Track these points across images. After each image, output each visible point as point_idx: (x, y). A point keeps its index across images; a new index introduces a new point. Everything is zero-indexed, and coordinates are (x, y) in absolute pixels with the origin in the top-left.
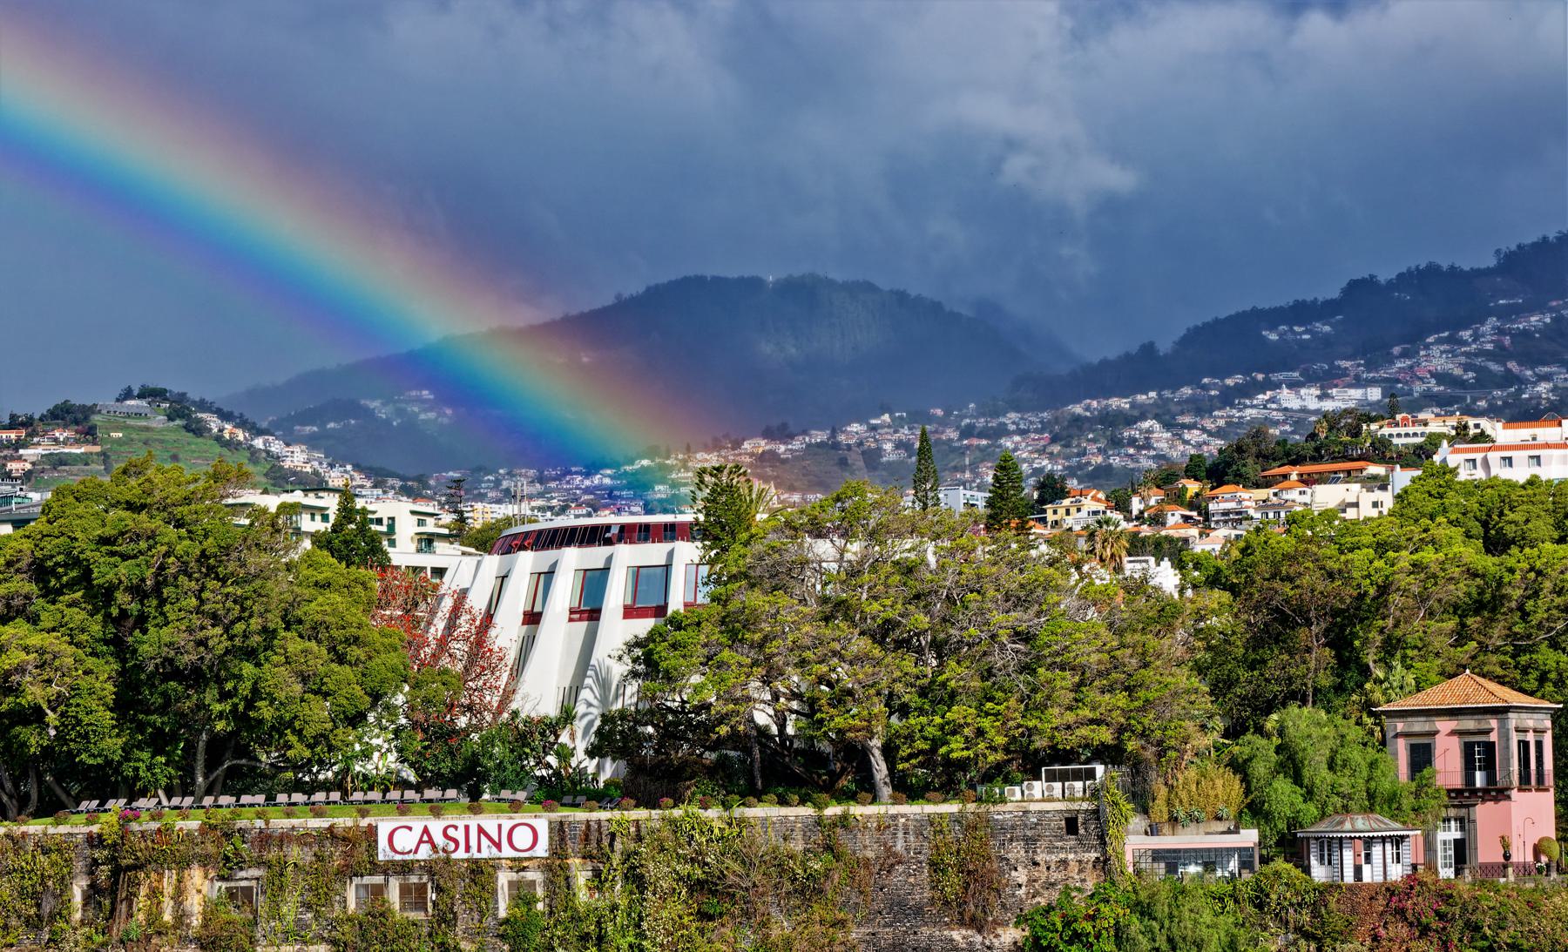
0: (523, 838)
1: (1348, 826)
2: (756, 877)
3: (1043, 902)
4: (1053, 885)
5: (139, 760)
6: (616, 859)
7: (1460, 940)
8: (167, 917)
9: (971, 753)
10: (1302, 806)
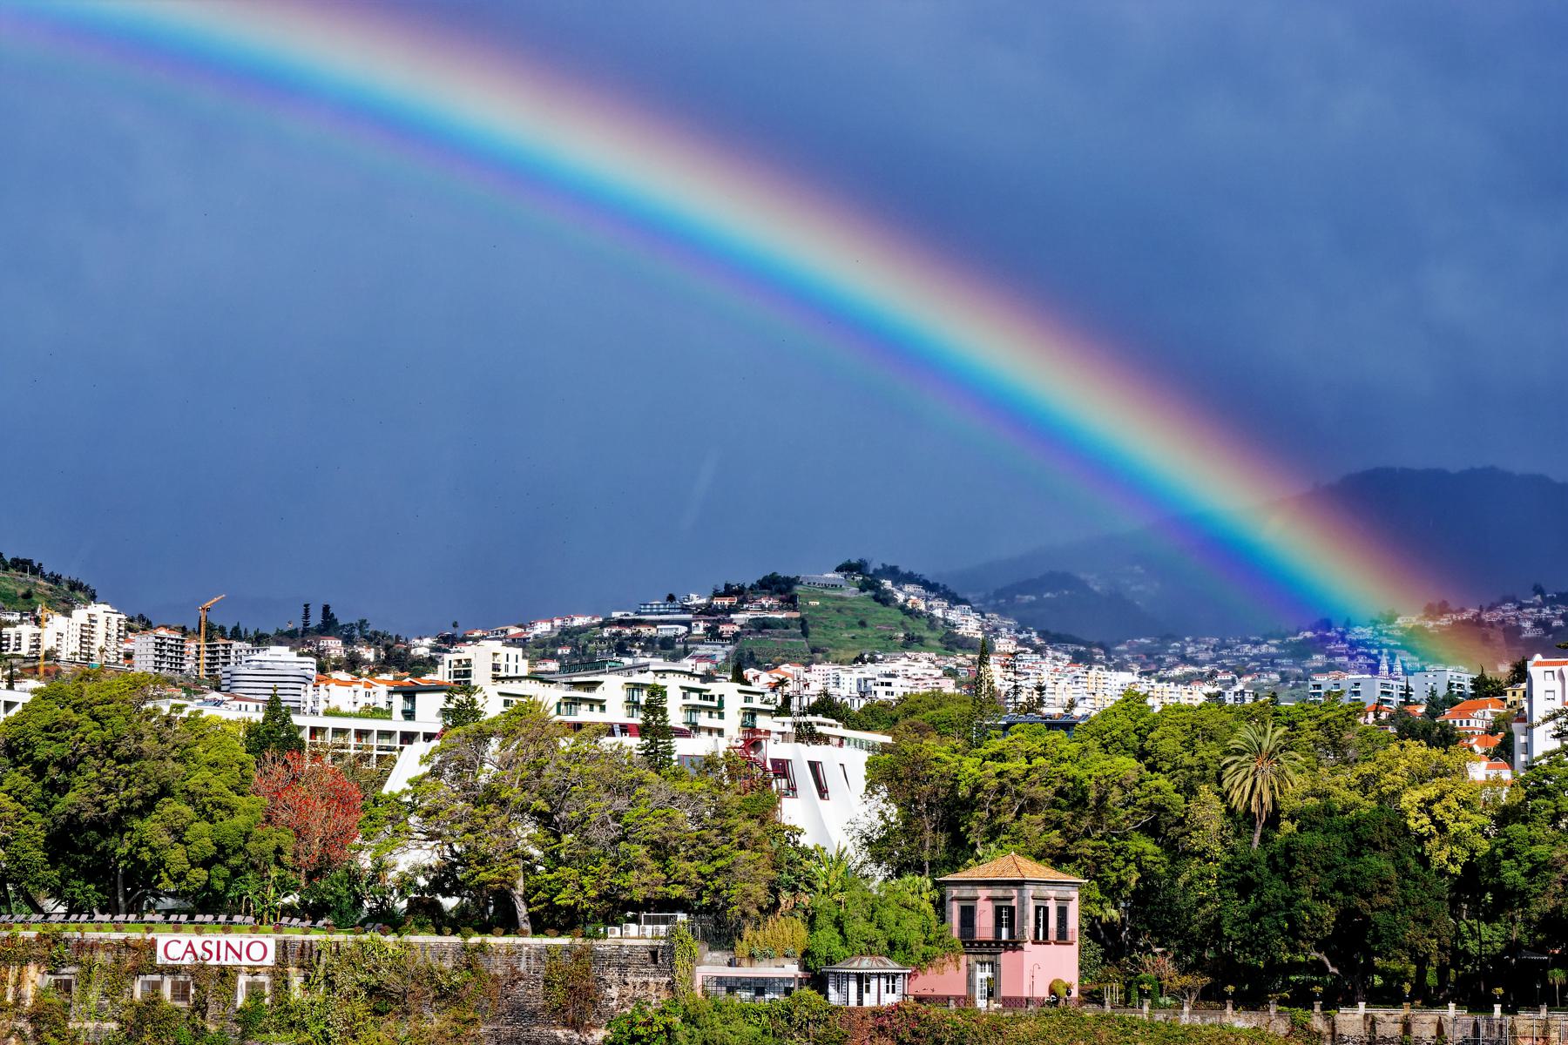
0: (256, 952)
1: (855, 964)
6: (321, 968)
8: (9, 999)
9: (572, 902)
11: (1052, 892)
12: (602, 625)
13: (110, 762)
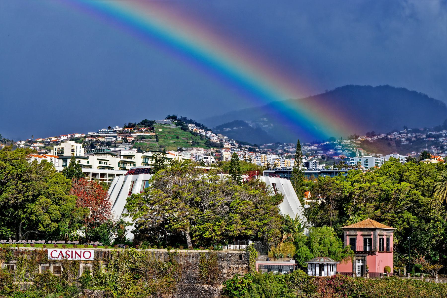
0: (87, 255)
1: (318, 260)
2: (149, 268)
3: (231, 278)
4: (234, 273)
5: (3, 230)
6: (112, 262)
7: (348, 294)
9: (210, 236)
10: (309, 254)
11: (385, 233)
12: (85, 137)
13: (19, 182)
